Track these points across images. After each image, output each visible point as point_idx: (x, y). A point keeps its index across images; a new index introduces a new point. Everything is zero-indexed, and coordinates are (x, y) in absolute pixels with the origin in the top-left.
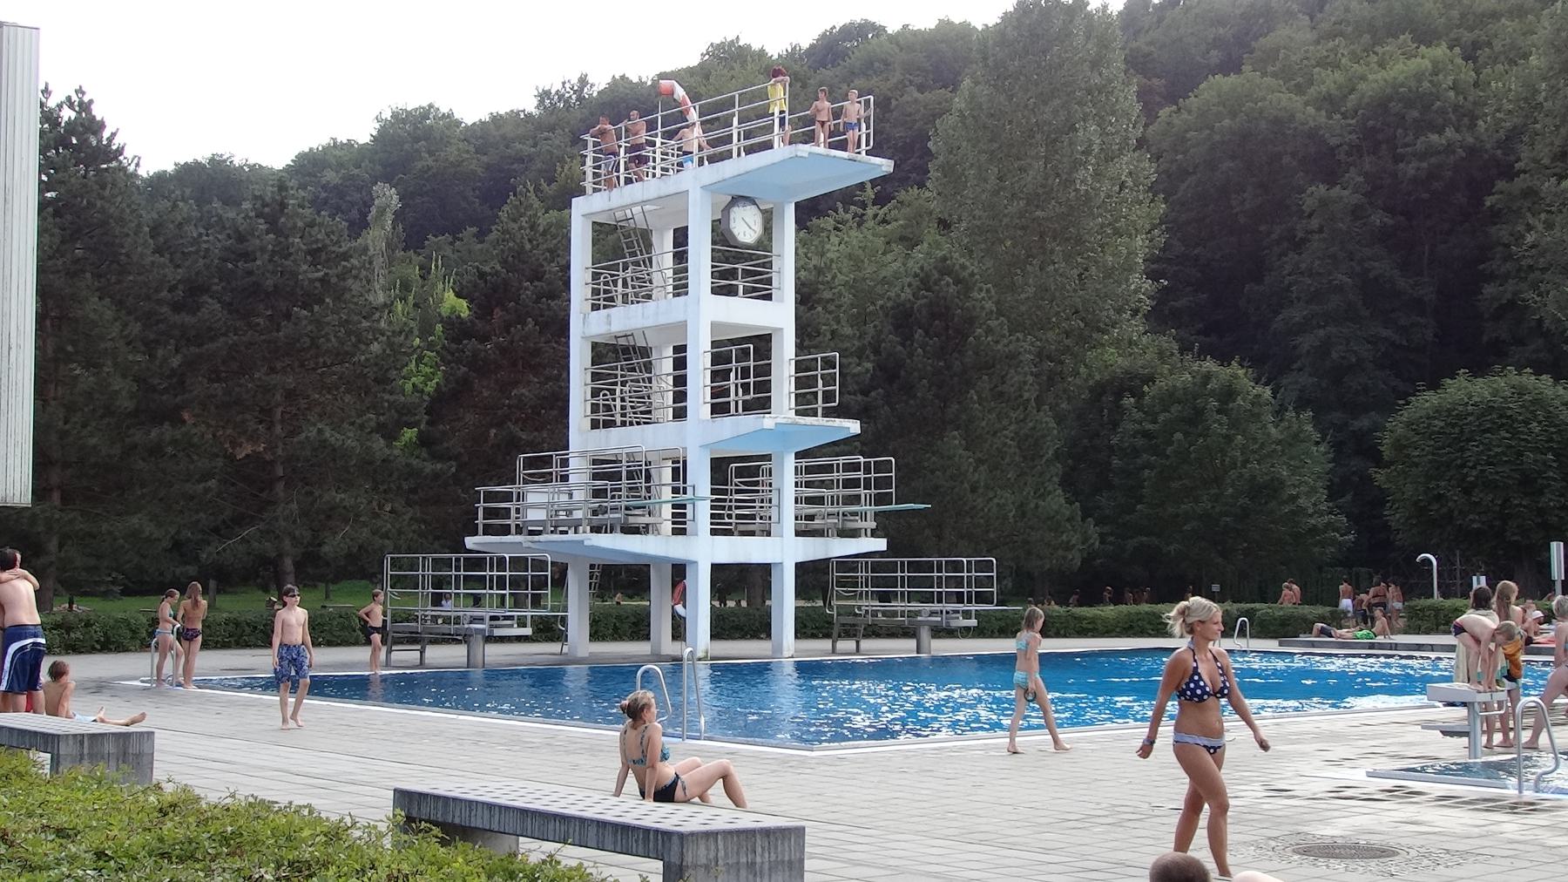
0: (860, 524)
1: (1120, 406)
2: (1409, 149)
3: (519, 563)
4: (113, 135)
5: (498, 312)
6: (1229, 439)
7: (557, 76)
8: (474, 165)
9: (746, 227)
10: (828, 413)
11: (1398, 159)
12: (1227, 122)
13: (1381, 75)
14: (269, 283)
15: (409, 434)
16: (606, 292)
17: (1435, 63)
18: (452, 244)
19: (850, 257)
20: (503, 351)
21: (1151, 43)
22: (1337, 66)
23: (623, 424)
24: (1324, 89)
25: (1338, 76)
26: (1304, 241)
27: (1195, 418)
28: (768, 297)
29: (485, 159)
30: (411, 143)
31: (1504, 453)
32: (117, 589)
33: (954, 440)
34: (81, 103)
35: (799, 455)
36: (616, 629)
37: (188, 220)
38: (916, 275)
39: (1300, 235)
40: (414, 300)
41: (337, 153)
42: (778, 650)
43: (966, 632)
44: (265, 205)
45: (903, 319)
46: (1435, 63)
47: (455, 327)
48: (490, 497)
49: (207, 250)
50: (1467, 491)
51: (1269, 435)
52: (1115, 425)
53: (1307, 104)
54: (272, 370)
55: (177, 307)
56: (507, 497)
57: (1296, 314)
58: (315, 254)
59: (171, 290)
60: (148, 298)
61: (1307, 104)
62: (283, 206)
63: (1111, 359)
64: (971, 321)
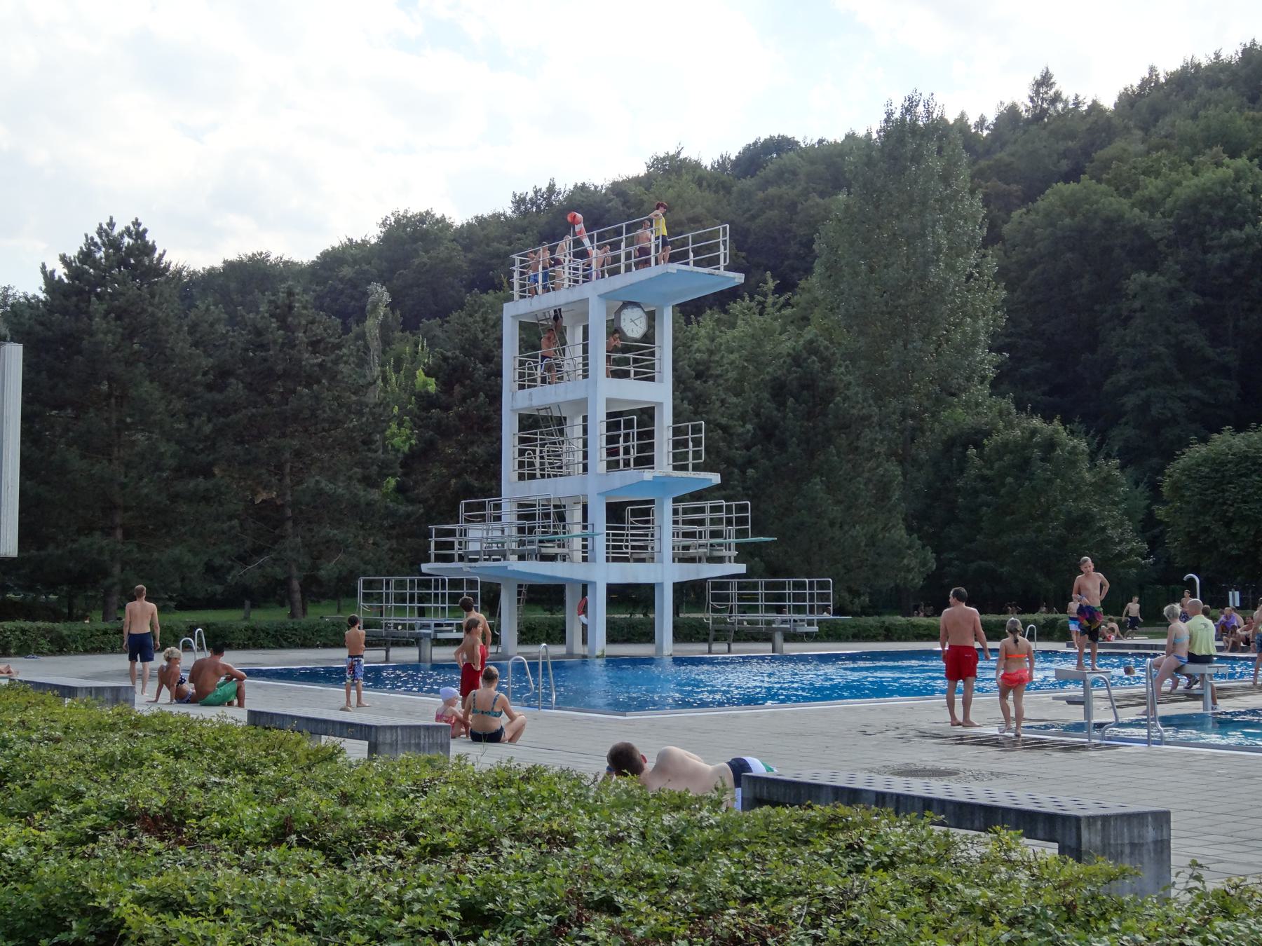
0: (725, 553)
1: (965, 456)
2: (1215, 242)
3: (456, 583)
4: (161, 256)
5: (457, 388)
6: (1050, 481)
7: (529, 182)
8: (461, 260)
9: (634, 325)
10: (696, 468)
11: (1206, 251)
12: (1067, 221)
13: (1196, 180)
14: (279, 368)
15: (392, 482)
16: (530, 375)
17: (1237, 172)
18: (441, 326)
19: (753, 336)
20: (461, 418)
21: (1013, 155)
22: (1158, 174)
23: (543, 476)
24: (1146, 193)
25: (1160, 183)
26: (1129, 318)
27: (1024, 465)
28: (652, 379)
29: (470, 256)
30: (411, 239)
31: (1255, 493)
32: (172, 604)
33: (817, 485)
34: (137, 233)
35: (675, 500)
36: (548, 635)
37: (218, 320)
38: (789, 355)
39: (1125, 313)
40: (393, 376)
41: (353, 251)
42: (660, 649)
43: (810, 637)
44: (277, 308)
45: (779, 390)
46: (1237, 172)
47: (427, 401)
48: (441, 533)
49: (233, 344)
50: (1228, 524)
51: (1082, 478)
52: (962, 471)
53: (1133, 205)
54: (284, 435)
55: (210, 387)
56: (451, 533)
57: (1122, 378)
58: (315, 345)
59: (205, 374)
60: (187, 381)
61: (1133, 205)
62: (291, 307)
63: (958, 417)
64: (832, 391)
